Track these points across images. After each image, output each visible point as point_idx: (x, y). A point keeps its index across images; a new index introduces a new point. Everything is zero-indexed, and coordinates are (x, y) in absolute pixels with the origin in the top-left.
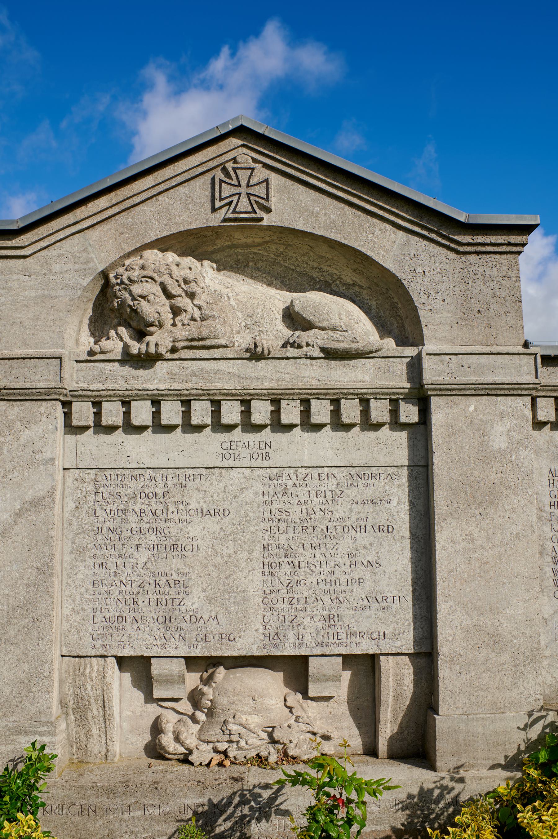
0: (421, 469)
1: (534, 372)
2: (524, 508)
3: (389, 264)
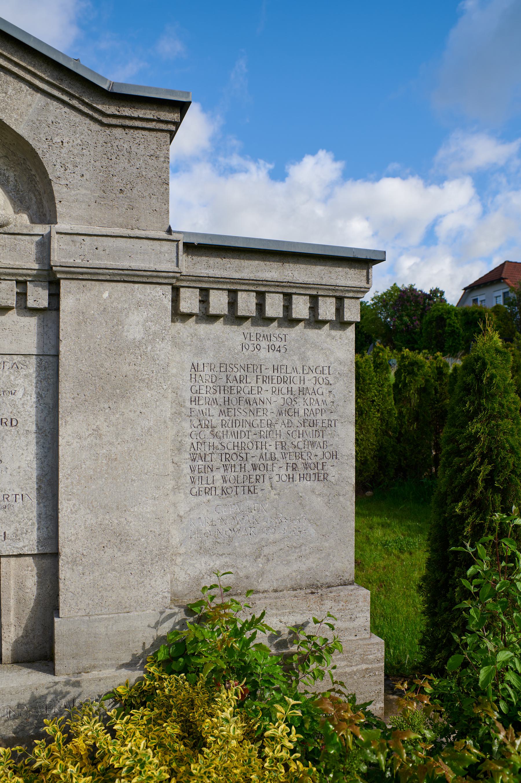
0: (51, 359)
1: (175, 260)
2: (158, 403)
3: (21, 130)
